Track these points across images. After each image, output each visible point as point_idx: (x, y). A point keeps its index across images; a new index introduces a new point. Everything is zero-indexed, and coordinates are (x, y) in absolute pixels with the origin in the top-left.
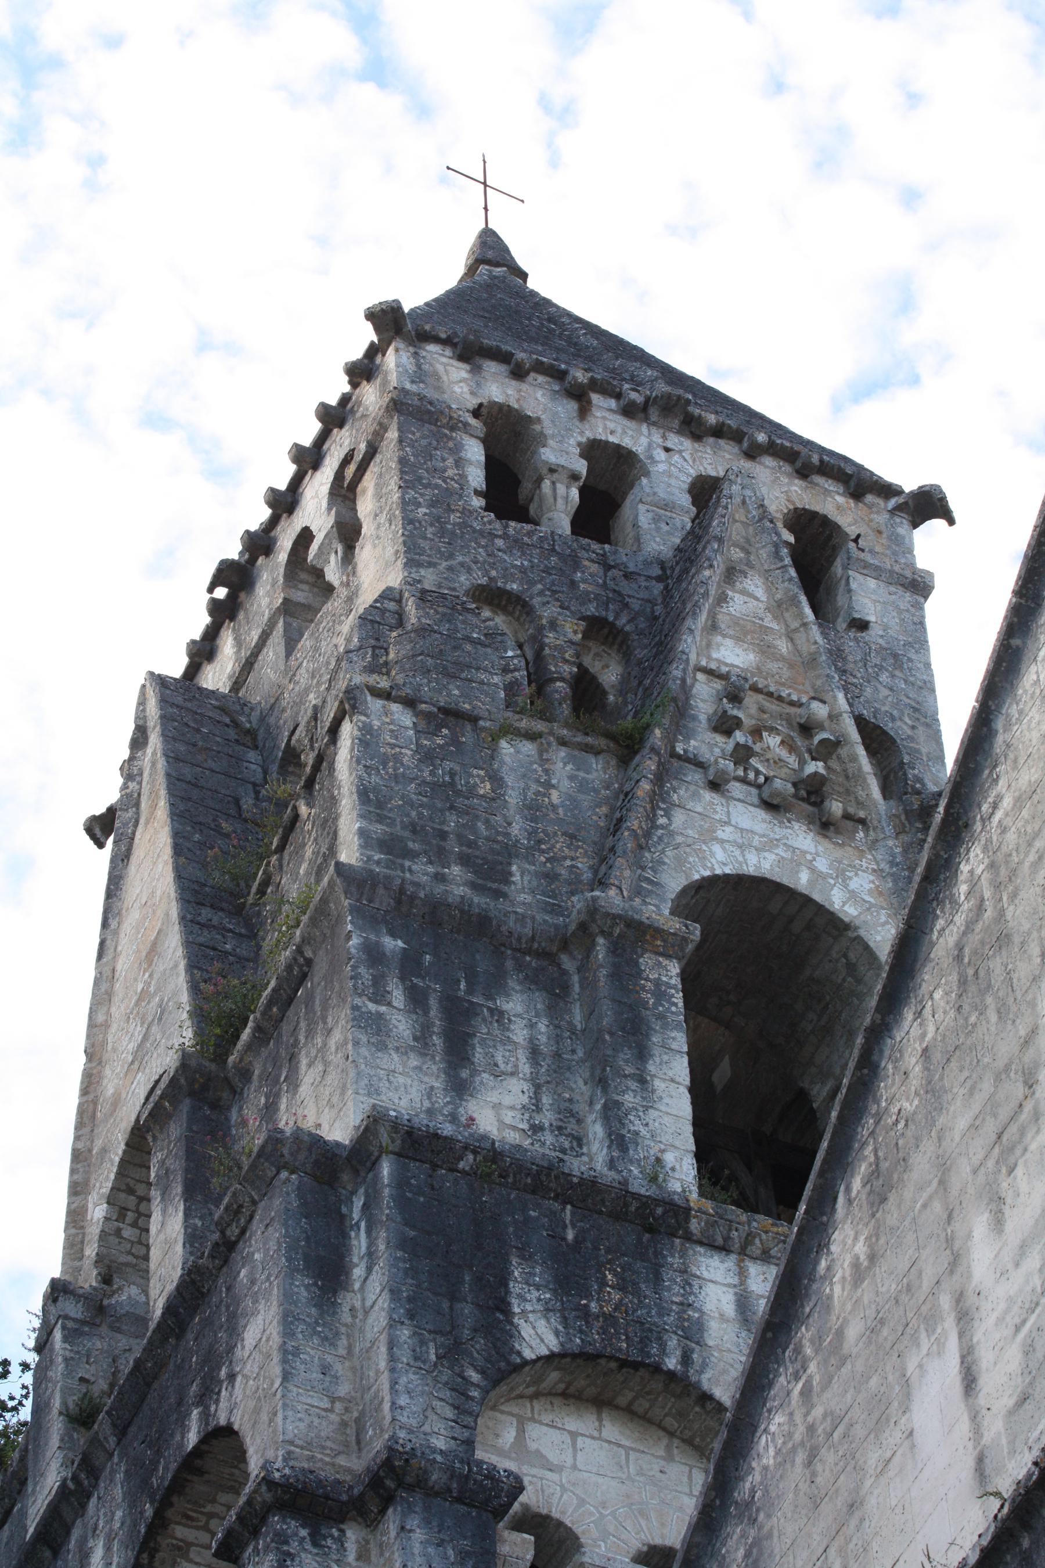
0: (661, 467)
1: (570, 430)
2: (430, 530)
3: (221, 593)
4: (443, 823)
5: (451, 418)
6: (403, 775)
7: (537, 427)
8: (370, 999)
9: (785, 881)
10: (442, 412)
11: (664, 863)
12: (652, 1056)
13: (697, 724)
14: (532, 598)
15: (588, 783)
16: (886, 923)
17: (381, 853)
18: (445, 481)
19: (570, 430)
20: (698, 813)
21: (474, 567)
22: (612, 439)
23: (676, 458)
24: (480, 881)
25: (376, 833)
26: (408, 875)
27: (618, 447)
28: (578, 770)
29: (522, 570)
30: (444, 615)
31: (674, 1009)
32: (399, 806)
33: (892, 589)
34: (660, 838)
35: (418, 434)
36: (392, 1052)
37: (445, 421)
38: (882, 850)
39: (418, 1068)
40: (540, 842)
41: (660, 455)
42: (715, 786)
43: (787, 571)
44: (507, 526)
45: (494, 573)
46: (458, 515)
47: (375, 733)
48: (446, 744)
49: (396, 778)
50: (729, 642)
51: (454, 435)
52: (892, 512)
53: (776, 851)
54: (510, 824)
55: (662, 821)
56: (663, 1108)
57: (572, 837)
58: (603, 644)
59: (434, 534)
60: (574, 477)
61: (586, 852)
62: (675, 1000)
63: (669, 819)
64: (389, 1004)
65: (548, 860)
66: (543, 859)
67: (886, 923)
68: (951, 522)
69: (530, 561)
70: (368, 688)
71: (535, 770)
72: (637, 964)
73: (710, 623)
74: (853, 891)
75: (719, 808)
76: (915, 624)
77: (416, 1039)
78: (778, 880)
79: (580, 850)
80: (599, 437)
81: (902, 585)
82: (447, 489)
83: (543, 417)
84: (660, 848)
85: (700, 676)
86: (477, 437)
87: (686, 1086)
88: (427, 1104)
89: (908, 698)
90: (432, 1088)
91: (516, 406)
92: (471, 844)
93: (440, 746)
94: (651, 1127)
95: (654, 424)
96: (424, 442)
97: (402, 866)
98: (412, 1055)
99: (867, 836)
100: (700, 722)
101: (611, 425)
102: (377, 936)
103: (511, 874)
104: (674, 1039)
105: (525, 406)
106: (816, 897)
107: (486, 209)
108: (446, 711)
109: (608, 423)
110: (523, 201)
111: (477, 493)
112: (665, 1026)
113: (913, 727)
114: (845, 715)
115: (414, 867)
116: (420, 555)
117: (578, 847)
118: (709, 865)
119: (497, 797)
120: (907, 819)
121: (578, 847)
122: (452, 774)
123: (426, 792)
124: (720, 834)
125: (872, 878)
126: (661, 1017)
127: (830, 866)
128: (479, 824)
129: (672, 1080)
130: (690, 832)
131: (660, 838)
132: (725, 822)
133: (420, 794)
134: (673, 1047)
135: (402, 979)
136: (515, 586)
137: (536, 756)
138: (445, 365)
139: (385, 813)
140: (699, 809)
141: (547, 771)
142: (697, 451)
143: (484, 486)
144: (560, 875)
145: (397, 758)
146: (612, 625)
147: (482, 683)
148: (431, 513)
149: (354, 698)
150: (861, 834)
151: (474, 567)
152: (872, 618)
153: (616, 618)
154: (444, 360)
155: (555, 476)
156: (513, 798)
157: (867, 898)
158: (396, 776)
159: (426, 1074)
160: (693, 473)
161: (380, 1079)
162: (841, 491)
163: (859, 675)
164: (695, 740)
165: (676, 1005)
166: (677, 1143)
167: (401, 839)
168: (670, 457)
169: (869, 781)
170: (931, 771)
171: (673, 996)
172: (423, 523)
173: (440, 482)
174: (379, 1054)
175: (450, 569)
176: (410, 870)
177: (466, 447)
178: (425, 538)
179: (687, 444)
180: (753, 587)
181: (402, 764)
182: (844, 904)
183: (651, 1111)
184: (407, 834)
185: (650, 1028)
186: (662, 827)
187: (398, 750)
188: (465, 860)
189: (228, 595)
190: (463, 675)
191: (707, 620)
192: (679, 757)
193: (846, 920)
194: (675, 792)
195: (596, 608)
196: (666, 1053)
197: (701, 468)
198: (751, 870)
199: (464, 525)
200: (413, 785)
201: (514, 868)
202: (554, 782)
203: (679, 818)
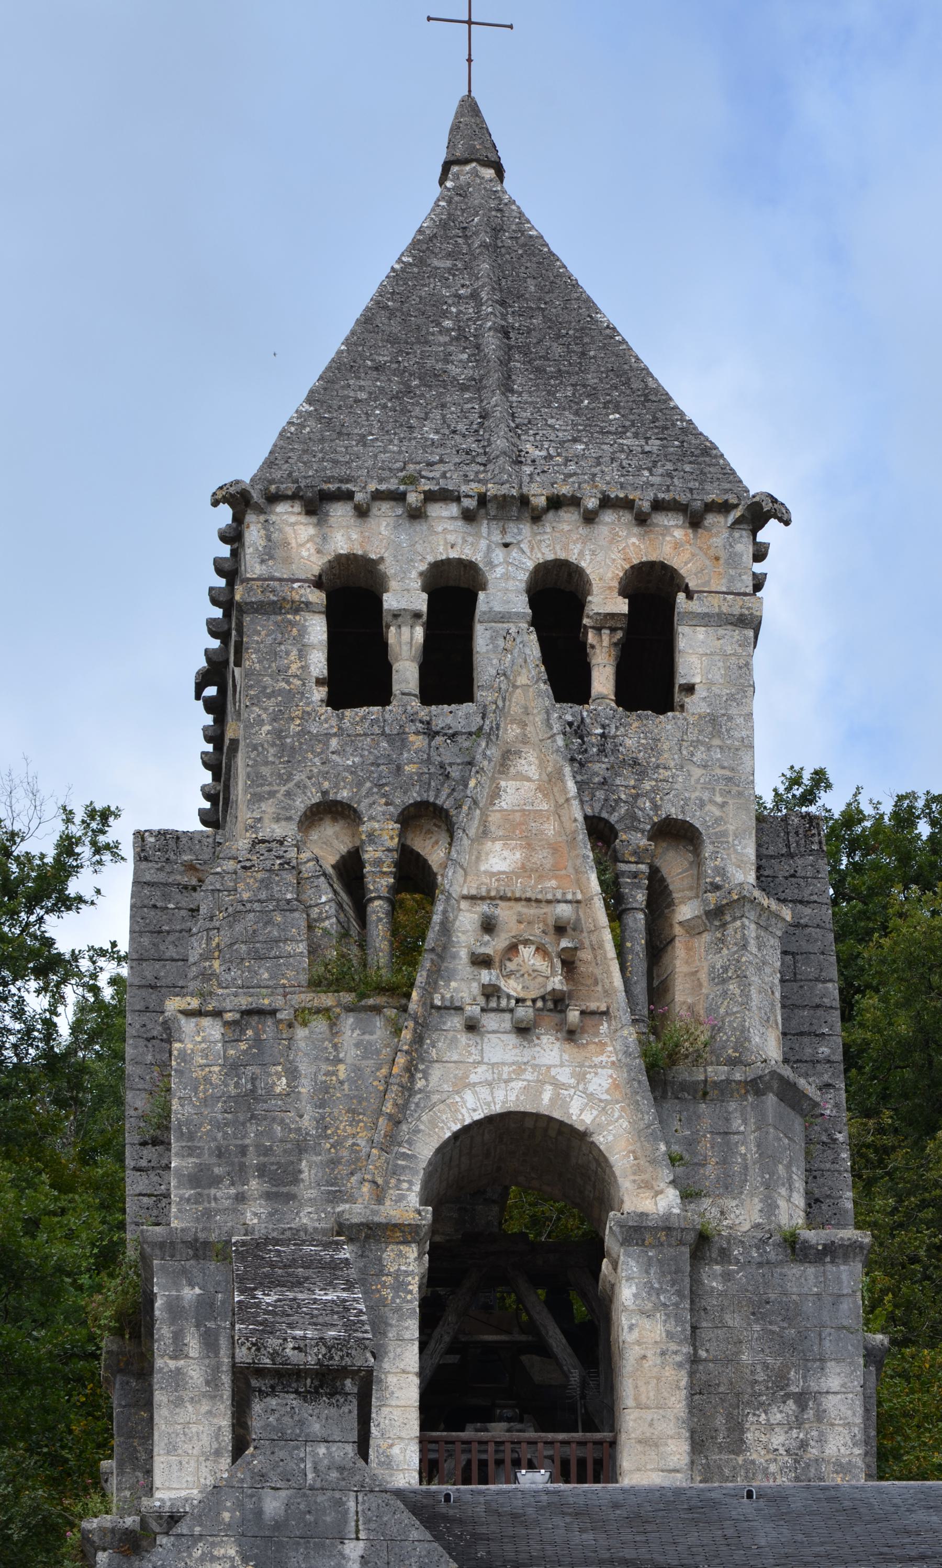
0: (500, 571)
1: (412, 560)
2: (272, 751)
3: (211, 691)
4: (244, 1137)
5: (293, 602)
6: (212, 1096)
7: (382, 567)
8: (171, 1358)
9: (529, 1108)
10: (284, 599)
11: (419, 1131)
12: (386, 1353)
13: (457, 961)
14: (359, 802)
15: (371, 1045)
16: (620, 1117)
17: (192, 1188)
18: (288, 683)
19: (412, 560)
20: (455, 1062)
21: (309, 783)
22: (453, 554)
23: (515, 553)
24: (274, 1189)
25: (187, 1168)
26: (213, 1204)
27: (460, 560)
28: (363, 1034)
29: (352, 770)
30: (262, 881)
31: (409, 1297)
32: (208, 1131)
33: (721, 631)
34: (417, 1105)
35: (263, 633)
36: (187, 1404)
37: (288, 606)
38: (620, 1041)
39: (209, 1412)
40: (326, 1128)
41: (499, 555)
42: (472, 1027)
43: (555, 741)
44: (341, 719)
45: (326, 785)
46: (298, 722)
47: (188, 1058)
48: (250, 1048)
49: (205, 1102)
50: (498, 845)
51: (298, 618)
52: (733, 526)
53: (523, 1077)
54: (301, 1116)
55: (420, 1084)
56: (394, 1403)
57: (353, 1111)
58: (434, 818)
59: (275, 756)
60: (417, 615)
61: (365, 1123)
62: (410, 1287)
63: (427, 1080)
64: (187, 1357)
65: (332, 1146)
66: (328, 1146)
67: (620, 1117)
68: (787, 523)
69: (362, 756)
70: (181, 1012)
71: (326, 1048)
72: (380, 1259)
73: (482, 828)
74: (592, 1094)
75: (473, 1050)
76: (740, 668)
77: (208, 1383)
78: (522, 1109)
79: (361, 1124)
80: (440, 558)
81: (731, 624)
82: (290, 690)
83: (386, 555)
84: (416, 1115)
85: (464, 905)
86: (320, 612)
87: (416, 1374)
88: (215, 1445)
89: (723, 768)
90: (220, 1428)
91: (360, 553)
92: (267, 1151)
93: (245, 1052)
94: (382, 1426)
95: (495, 518)
96: (269, 640)
97: (208, 1196)
98: (204, 1401)
99: (609, 1025)
100: (461, 959)
101: (451, 538)
102: (178, 1291)
103: (300, 1172)
104: (407, 1328)
105: (368, 548)
106: (556, 1115)
107: (470, 60)
108: (248, 1013)
109: (449, 537)
110: (511, 27)
111: (319, 682)
112: (401, 1318)
113: (723, 805)
114: (596, 898)
115: (219, 1194)
116: (262, 785)
117: (360, 1121)
118: (460, 1117)
119: (291, 1093)
120: (707, 918)
121: (360, 1121)
122: (253, 1079)
123: (231, 1107)
124: (473, 1078)
125: (610, 1071)
126: (398, 1310)
127: (573, 1075)
128: (275, 1126)
129: (404, 1372)
130: (446, 1087)
131: (417, 1105)
132: (478, 1063)
133: (226, 1112)
134: (406, 1337)
135: (198, 1326)
136: (345, 794)
137: (328, 1032)
138: (293, 525)
139: (196, 1144)
140: (455, 1057)
141: (335, 1046)
142: (536, 534)
143: (325, 672)
144: (342, 1157)
145: (206, 1080)
146: (434, 804)
147: (290, 956)
148: (274, 728)
149: (169, 1028)
150: (605, 1025)
151: (309, 783)
152: (697, 680)
153: (437, 797)
154: (293, 519)
155: (400, 619)
156: (305, 1088)
157: (605, 1097)
158: (205, 1099)
159: (215, 1416)
160: (530, 565)
161: (177, 1435)
162: (681, 522)
163: (672, 764)
164: (455, 980)
165: (411, 1292)
166: (403, 1435)
167: (209, 1168)
168: (508, 554)
169: (612, 969)
170: (736, 851)
171: (409, 1284)
172: (266, 746)
173: (283, 685)
174: (178, 1410)
175: (288, 794)
176: (215, 1199)
177: (310, 629)
178: (266, 763)
179: (526, 529)
180: (526, 768)
181: (211, 1084)
182: (582, 1111)
183: (383, 1409)
184: (214, 1160)
185: (387, 1324)
186: (420, 1091)
187: (207, 1069)
188: (262, 1171)
189: (218, 691)
190: (272, 954)
191: (478, 828)
192: (439, 1008)
193: (581, 1128)
194: (434, 1047)
195: (419, 793)
196: (399, 1346)
197: (539, 555)
198: (498, 1109)
199: (304, 732)
200: (220, 1105)
201: (304, 1163)
202: (341, 1055)
203: (436, 1073)
